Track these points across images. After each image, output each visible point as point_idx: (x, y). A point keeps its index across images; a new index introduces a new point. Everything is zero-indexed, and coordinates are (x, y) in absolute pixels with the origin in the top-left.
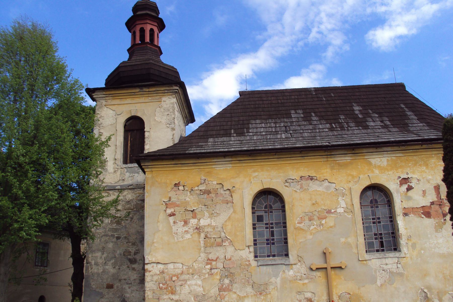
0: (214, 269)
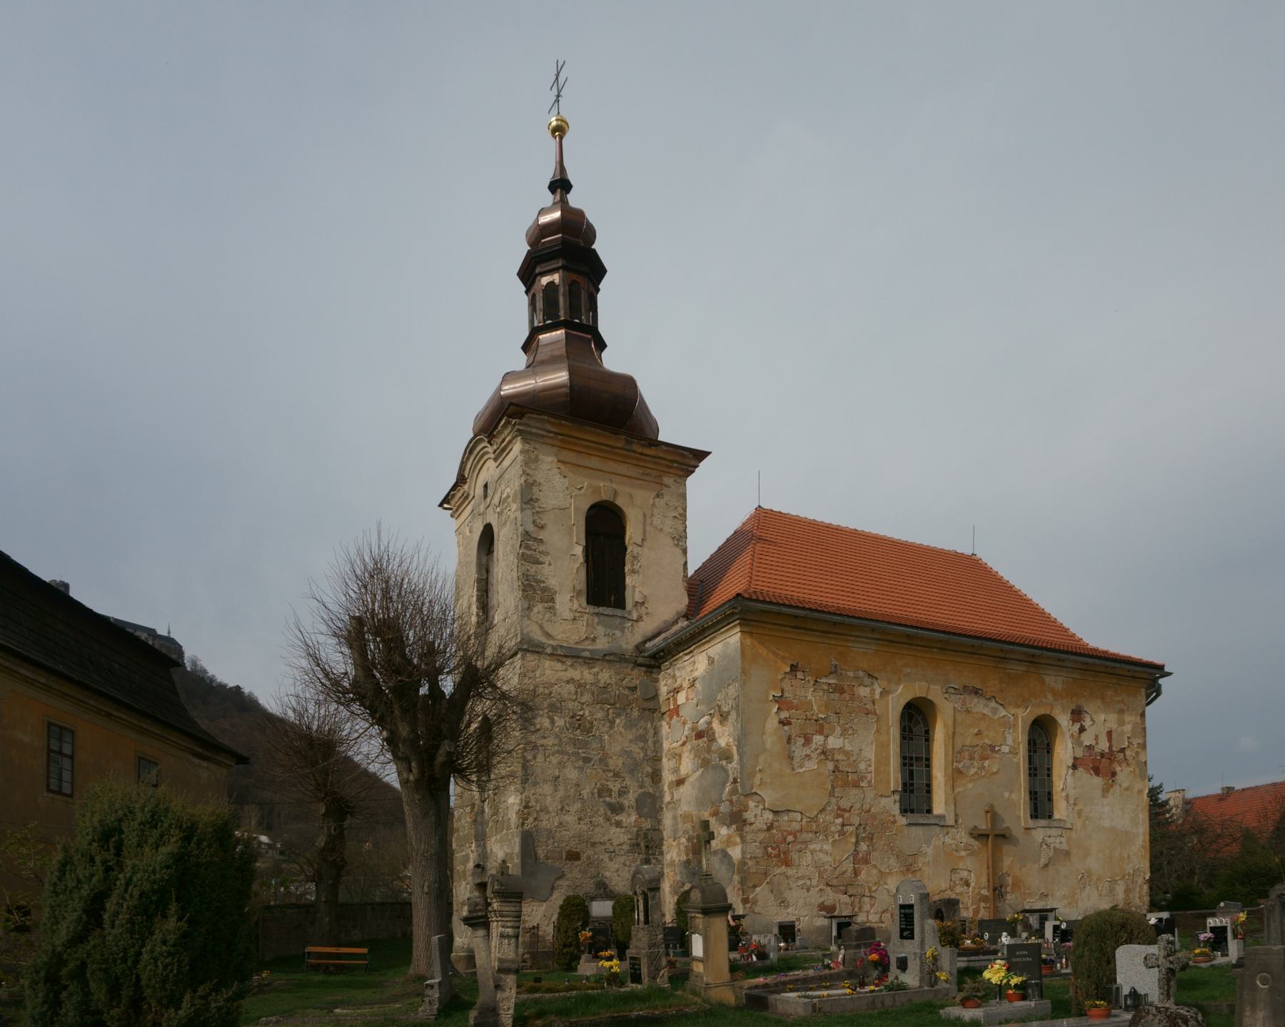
0: (847, 825)
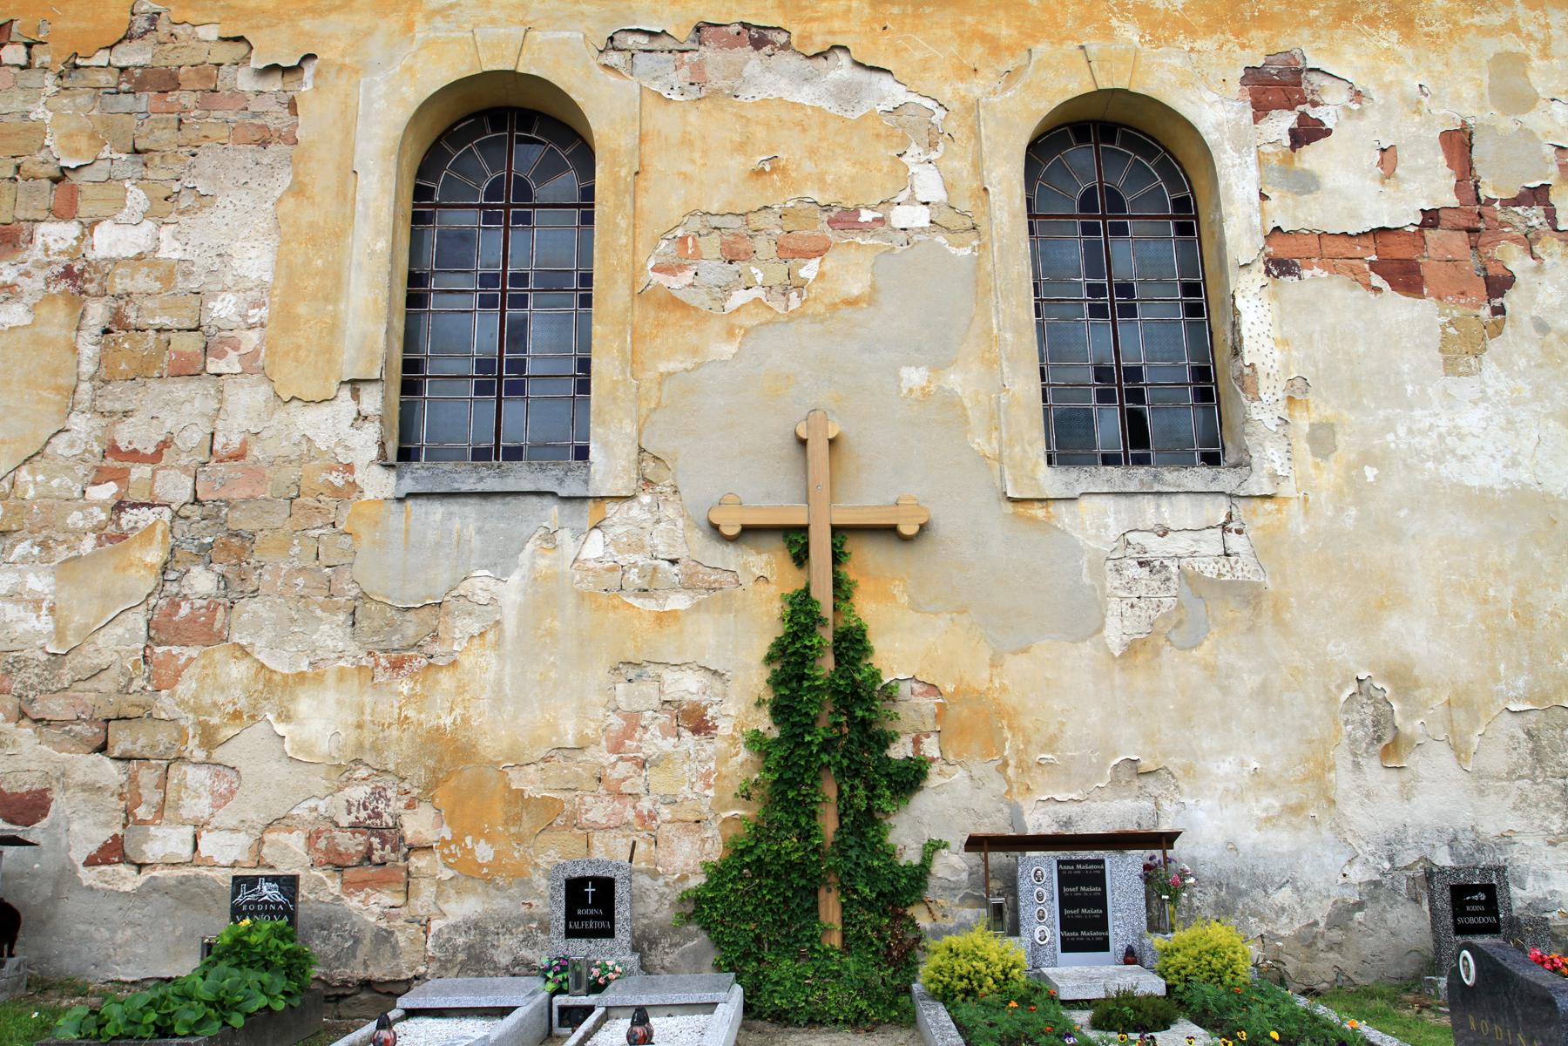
0: (134, 506)
